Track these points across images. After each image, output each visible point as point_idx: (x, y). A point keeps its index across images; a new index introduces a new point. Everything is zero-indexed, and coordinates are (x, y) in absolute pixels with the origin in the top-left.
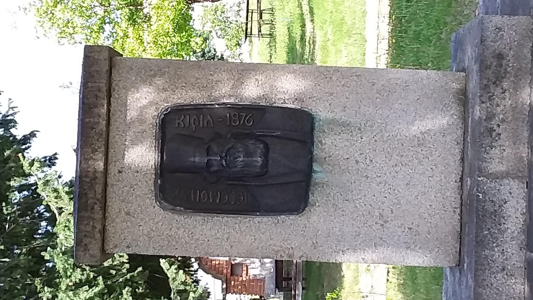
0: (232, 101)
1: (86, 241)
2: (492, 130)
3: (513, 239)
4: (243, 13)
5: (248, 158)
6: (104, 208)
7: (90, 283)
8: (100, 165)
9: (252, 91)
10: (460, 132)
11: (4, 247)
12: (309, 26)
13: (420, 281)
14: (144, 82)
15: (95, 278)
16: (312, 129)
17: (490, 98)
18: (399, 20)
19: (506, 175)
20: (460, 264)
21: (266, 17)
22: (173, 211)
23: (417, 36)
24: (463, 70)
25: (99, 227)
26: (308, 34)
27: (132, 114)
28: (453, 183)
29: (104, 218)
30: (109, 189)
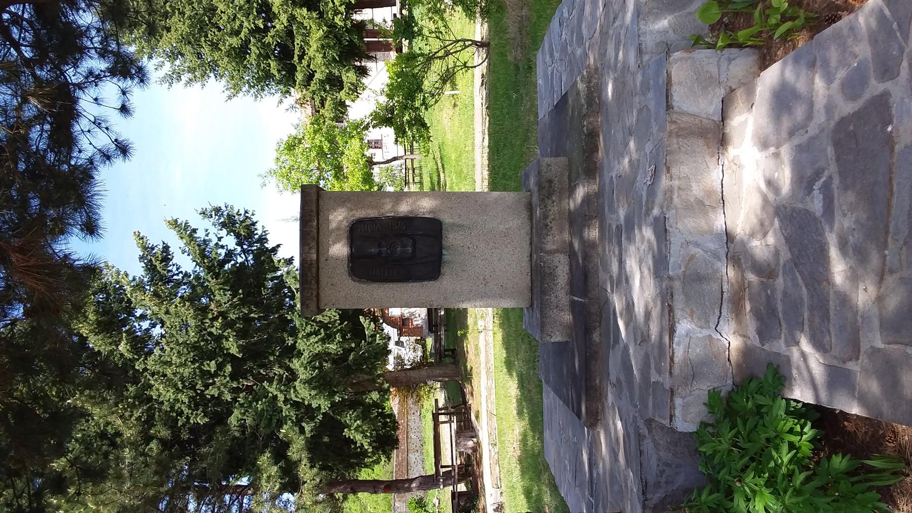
0: (392, 214)
1: (308, 302)
2: (547, 225)
3: (562, 289)
4: (404, 171)
5: (404, 249)
6: (318, 282)
7: (316, 333)
8: (314, 256)
9: (404, 208)
10: (529, 228)
11: (466, 486)
12: (442, 175)
13: (512, 320)
14: (339, 205)
15: (319, 330)
16: (441, 229)
17: (545, 206)
18: (493, 167)
19: (557, 251)
20: (532, 305)
21: (417, 171)
22: (360, 282)
23: (504, 175)
24: (530, 191)
25: (315, 293)
26: (442, 180)
27: (333, 225)
28: (526, 259)
29: (318, 288)
30: (320, 270)
